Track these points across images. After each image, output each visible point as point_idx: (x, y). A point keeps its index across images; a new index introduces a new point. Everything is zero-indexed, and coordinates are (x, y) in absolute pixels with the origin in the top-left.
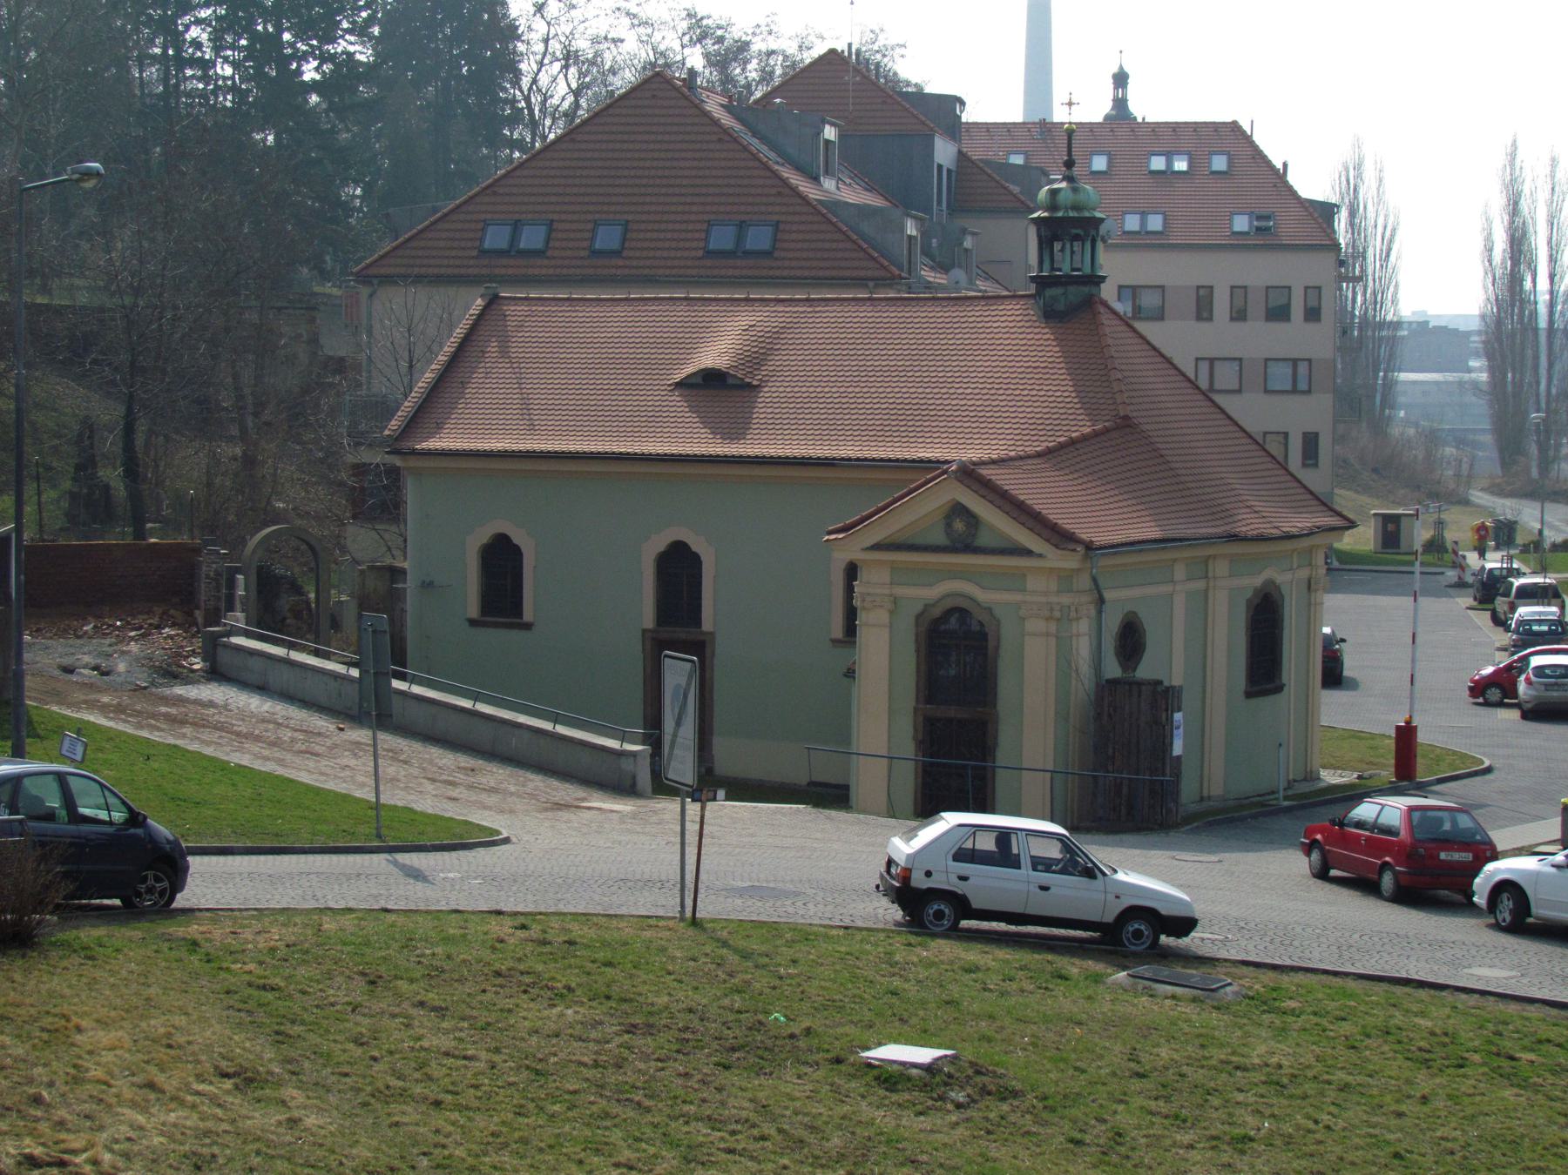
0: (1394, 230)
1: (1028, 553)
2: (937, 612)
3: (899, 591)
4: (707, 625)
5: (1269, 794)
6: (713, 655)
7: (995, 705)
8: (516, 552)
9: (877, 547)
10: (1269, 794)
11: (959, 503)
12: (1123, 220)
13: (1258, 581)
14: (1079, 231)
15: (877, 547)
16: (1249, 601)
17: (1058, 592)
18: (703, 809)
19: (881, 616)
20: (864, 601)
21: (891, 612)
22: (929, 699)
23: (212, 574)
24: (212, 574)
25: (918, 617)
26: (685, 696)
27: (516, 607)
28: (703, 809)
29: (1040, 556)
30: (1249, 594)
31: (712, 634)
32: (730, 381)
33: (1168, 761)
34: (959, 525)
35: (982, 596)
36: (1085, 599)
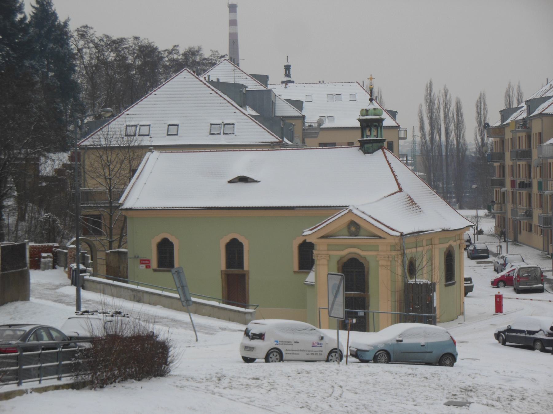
0: (381, 91)
1: (380, 237)
2: (345, 260)
3: (331, 253)
4: (246, 268)
5: (296, 351)
6: (249, 278)
7: (368, 292)
8: (240, 245)
9: (322, 237)
10: (296, 351)
11: (353, 221)
12: (547, 161)
13: (447, 245)
14: (376, 124)
15: (322, 237)
16: (445, 253)
17: (391, 251)
18: (505, 298)
19: (324, 261)
20: (318, 256)
21: (328, 261)
22: (346, 291)
23: (72, 255)
24: (72, 255)
25: (338, 262)
26: (339, 287)
27: (171, 265)
28: (505, 298)
29: (384, 238)
30: (445, 250)
31: (248, 271)
32: (249, 180)
33: (433, 308)
34: (353, 229)
35: (363, 253)
36: (399, 252)
